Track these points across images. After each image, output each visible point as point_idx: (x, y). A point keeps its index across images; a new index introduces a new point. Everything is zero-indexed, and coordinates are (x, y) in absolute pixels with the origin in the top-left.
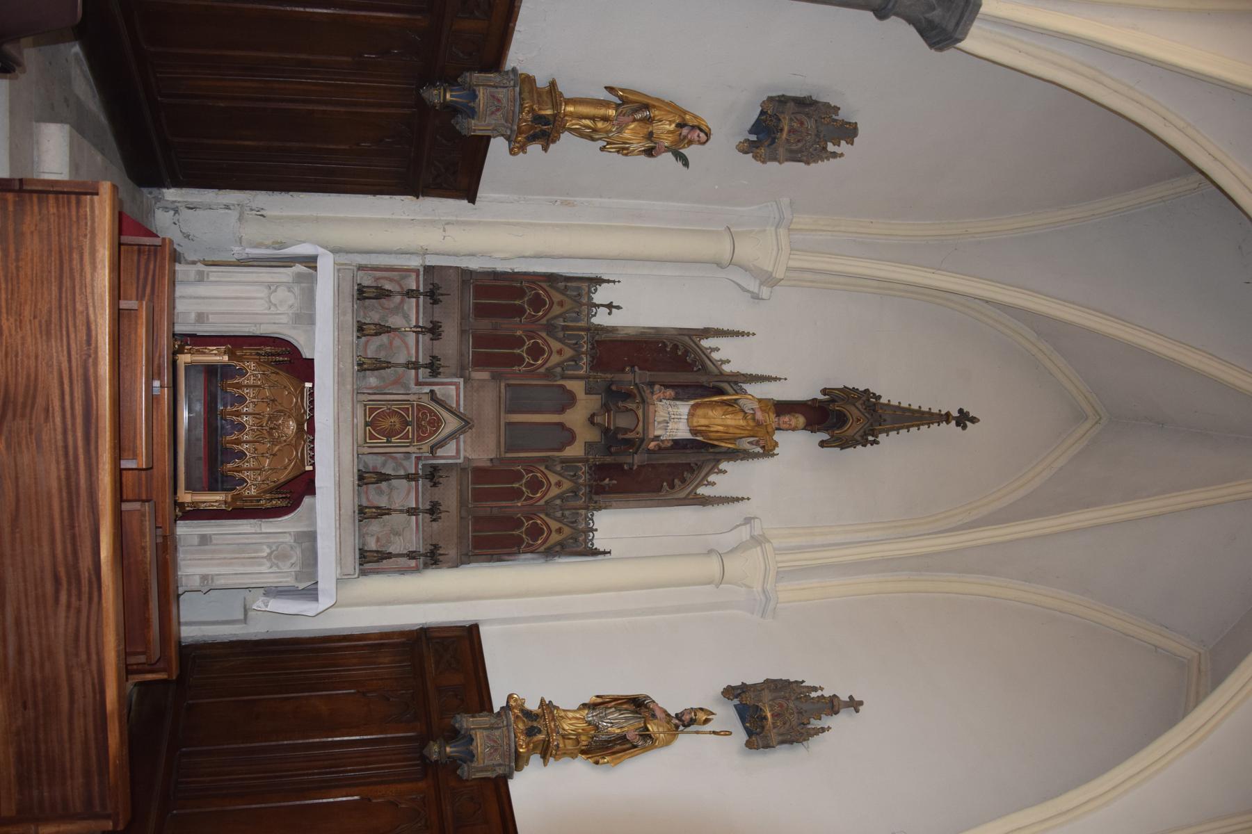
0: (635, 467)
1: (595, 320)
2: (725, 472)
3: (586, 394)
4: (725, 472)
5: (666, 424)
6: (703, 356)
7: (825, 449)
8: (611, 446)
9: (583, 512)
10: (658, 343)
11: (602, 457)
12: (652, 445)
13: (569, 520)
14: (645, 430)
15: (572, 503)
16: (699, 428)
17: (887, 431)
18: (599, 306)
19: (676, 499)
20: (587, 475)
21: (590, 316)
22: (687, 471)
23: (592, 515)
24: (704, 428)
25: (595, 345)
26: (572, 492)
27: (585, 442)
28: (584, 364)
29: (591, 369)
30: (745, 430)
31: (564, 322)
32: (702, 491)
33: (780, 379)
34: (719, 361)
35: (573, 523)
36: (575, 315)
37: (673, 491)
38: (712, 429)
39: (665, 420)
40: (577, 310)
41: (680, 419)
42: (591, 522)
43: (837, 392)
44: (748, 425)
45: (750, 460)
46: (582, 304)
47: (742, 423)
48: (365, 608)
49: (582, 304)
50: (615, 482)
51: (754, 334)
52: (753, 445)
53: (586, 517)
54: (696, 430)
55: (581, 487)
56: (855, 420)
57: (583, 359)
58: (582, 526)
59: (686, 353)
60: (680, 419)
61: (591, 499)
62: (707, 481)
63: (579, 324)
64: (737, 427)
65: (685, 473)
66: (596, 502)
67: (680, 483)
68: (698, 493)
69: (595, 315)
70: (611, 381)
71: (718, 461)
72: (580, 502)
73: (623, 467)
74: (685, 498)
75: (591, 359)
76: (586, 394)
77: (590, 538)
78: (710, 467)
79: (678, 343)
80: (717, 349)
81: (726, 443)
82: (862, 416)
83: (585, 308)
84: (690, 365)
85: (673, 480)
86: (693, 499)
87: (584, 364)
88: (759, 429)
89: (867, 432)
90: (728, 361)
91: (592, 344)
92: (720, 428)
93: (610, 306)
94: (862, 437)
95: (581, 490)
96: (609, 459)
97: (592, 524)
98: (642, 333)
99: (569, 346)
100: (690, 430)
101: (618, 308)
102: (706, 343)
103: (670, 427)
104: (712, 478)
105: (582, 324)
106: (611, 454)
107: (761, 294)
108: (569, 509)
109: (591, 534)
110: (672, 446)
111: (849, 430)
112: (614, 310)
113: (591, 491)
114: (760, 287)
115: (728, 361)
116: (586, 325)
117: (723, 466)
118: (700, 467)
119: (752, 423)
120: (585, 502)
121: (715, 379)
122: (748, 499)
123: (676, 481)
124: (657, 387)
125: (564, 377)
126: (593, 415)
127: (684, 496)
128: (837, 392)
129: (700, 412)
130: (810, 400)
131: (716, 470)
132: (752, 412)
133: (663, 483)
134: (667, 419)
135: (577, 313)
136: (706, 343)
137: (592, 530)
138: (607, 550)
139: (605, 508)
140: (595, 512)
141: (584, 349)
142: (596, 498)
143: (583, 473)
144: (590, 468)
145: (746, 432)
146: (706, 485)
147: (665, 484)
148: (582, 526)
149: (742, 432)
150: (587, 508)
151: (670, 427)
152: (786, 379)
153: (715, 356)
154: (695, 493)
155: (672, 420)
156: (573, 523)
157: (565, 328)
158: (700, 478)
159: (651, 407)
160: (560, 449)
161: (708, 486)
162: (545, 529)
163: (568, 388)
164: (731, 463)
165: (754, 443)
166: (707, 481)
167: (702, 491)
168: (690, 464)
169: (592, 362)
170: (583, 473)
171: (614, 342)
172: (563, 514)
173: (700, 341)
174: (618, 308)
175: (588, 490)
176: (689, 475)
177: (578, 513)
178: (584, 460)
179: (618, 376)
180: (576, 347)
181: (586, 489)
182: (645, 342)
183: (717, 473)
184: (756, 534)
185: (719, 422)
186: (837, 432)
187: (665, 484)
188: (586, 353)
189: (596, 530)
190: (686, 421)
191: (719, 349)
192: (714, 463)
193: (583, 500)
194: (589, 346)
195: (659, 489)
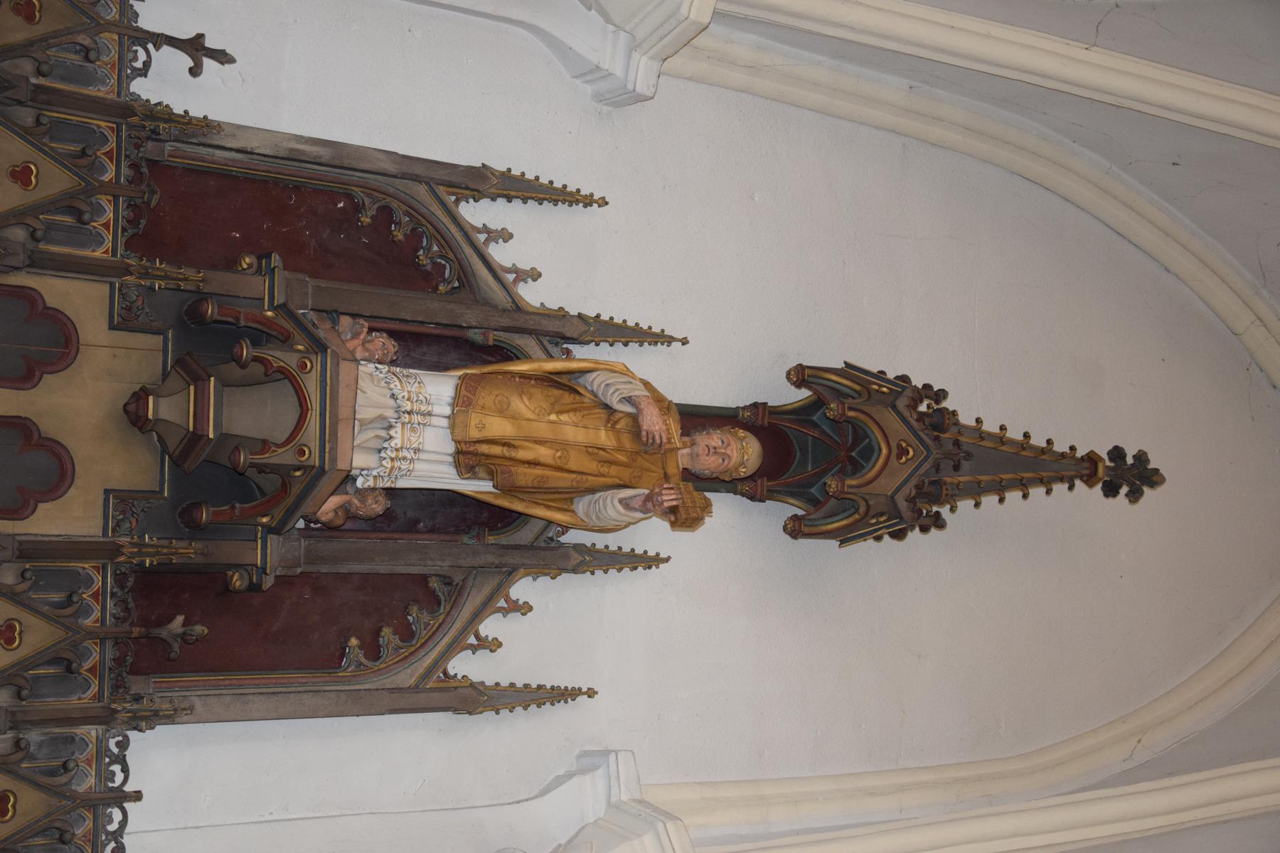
0: (268, 582)
1: (142, 88)
2: (525, 609)
3: (112, 327)
4: (525, 609)
5: (383, 433)
6: (468, 250)
7: (803, 542)
8: (197, 505)
9: (91, 732)
10: (333, 196)
11: (165, 542)
12: (330, 507)
13: (41, 764)
14: (328, 437)
15: (53, 703)
16: (484, 448)
17: (976, 492)
18: (161, 40)
19: (391, 690)
20: (109, 603)
21: (127, 71)
22: (416, 601)
23: (124, 745)
24: (496, 450)
25: (145, 170)
26: (55, 661)
27: (107, 492)
28: (106, 226)
29: (128, 245)
30: (611, 463)
31: (40, 73)
32: (464, 666)
33: (670, 340)
34: (509, 271)
35: (52, 773)
36: (76, 59)
37: (380, 664)
38: (521, 455)
39: (382, 418)
40: (87, 42)
41: (429, 414)
42: (116, 768)
43: (834, 378)
44: (619, 449)
45: (599, 573)
46: (101, 26)
47: (604, 437)
48: (456, 13)
49: (101, 26)
50: (200, 629)
51: (603, 202)
52: (635, 509)
53: (102, 751)
54: (475, 454)
55: (88, 644)
56: (895, 451)
57: (100, 211)
58: (87, 783)
59: (415, 237)
60: (429, 414)
61: (118, 686)
62: (477, 636)
63: (91, 91)
64: (593, 450)
65: (414, 609)
66: (138, 698)
67: (396, 640)
68: (451, 672)
69: (144, 72)
70: (199, 292)
71: (510, 574)
72: (83, 700)
73: (227, 583)
74: (415, 689)
75: (129, 214)
76: (112, 327)
77: (112, 827)
78: (486, 591)
79: (394, 204)
80: (505, 236)
81: (548, 507)
82: (915, 442)
83: (109, 39)
84: (427, 276)
85: (377, 632)
86: (439, 690)
87: (106, 226)
88: (647, 465)
89: (926, 488)
90: (535, 275)
91: (134, 166)
92: (544, 453)
93: (195, 47)
94: (910, 500)
95: (86, 654)
96: (188, 551)
97: (119, 777)
98: (293, 157)
99: (57, 158)
100: (458, 453)
101: (222, 57)
102: (476, 213)
103: (396, 442)
104: (490, 627)
105: (102, 91)
106: (195, 529)
107: (631, 78)
108: (43, 722)
109: (117, 815)
110: (388, 515)
111: (882, 480)
112: (208, 63)
113: (119, 661)
114: (629, 57)
115: (535, 275)
116: (113, 96)
117: (522, 589)
118: (456, 591)
119: (628, 444)
120: (99, 697)
121: (505, 322)
122: (591, 693)
123: (386, 631)
124: (345, 321)
125: (38, 263)
126: (140, 396)
127: (412, 681)
128: (834, 378)
129: (487, 397)
130: (744, 408)
131: (502, 603)
132: (629, 409)
133: (347, 640)
134: (390, 413)
135: (86, 52)
136: (476, 213)
137: (121, 798)
138: (663, 555)
139: (170, 719)
140: (132, 735)
141: (109, 176)
142: (137, 685)
143: (95, 596)
144: (120, 579)
145: (614, 470)
146: (474, 649)
147: (354, 642)
148: (87, 783)
149: (604, 470)
150: (106, 718)
151: (396, 442)
152: (684, 342)
153: (500, 254)
154: (445, 673)
155: (406, 418)
156: (52, 773)
157: (42, 97)
158: (458, 625)
159: (345, 367)
160: (18, 511)
161: (480, 652)
162: (317, 526)
163: (51, 301)
164: (544, 581)
165: (637, 503)
166: (477, 636)
167: (464, 666)
168: (424, 579)
169: (133, 222)
170: (95, 596)
171: (197, 173)
172: (17, 743)
173: (457, 202)
174: (222, 57)
175: (110, 654)
176: (426, 617)
177: (70, 740)
178: (102, 551)
179: (219, 281)
180: (82, 162)
181: (102, 653)
182: (297, 188)
183: (505, 612)
184: (624, 797)
185: (541, 430)
186: (854, 482)
187: (354, 642)
188: (112, 190)
189: (137, 796)
190: (445, 422)
191: (511, 236)
192: (496, 580)
193: (94, 689)
194: (125, 171)
195: (331, 661)
